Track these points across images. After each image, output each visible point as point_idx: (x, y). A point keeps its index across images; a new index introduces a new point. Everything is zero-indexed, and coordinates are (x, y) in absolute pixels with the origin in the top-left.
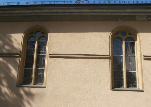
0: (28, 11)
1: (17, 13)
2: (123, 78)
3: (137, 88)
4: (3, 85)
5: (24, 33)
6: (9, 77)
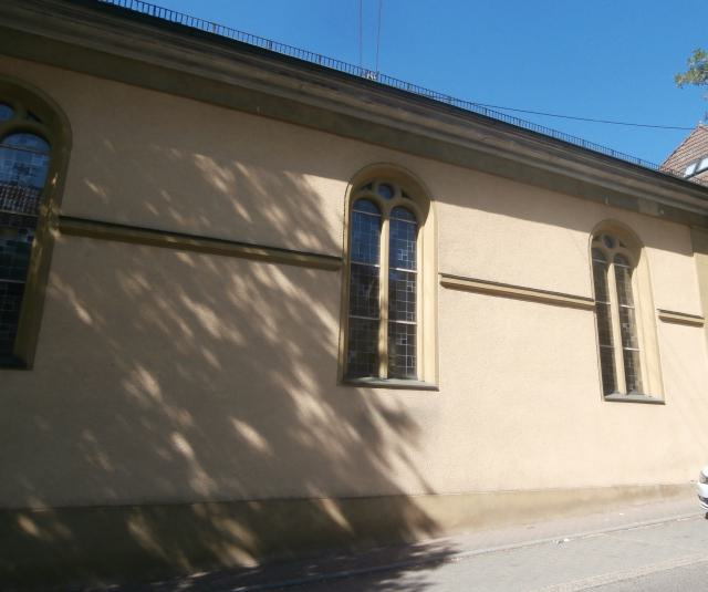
0: (373, 107)
1: (426, 128)
2: (618, 372)
3: (416, 379)
4: (298, 384)
5: (350, 183)
6: (314, 354)
